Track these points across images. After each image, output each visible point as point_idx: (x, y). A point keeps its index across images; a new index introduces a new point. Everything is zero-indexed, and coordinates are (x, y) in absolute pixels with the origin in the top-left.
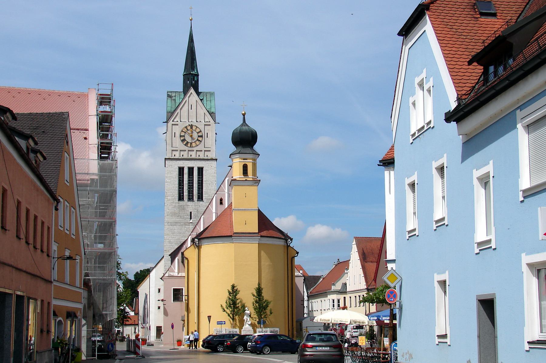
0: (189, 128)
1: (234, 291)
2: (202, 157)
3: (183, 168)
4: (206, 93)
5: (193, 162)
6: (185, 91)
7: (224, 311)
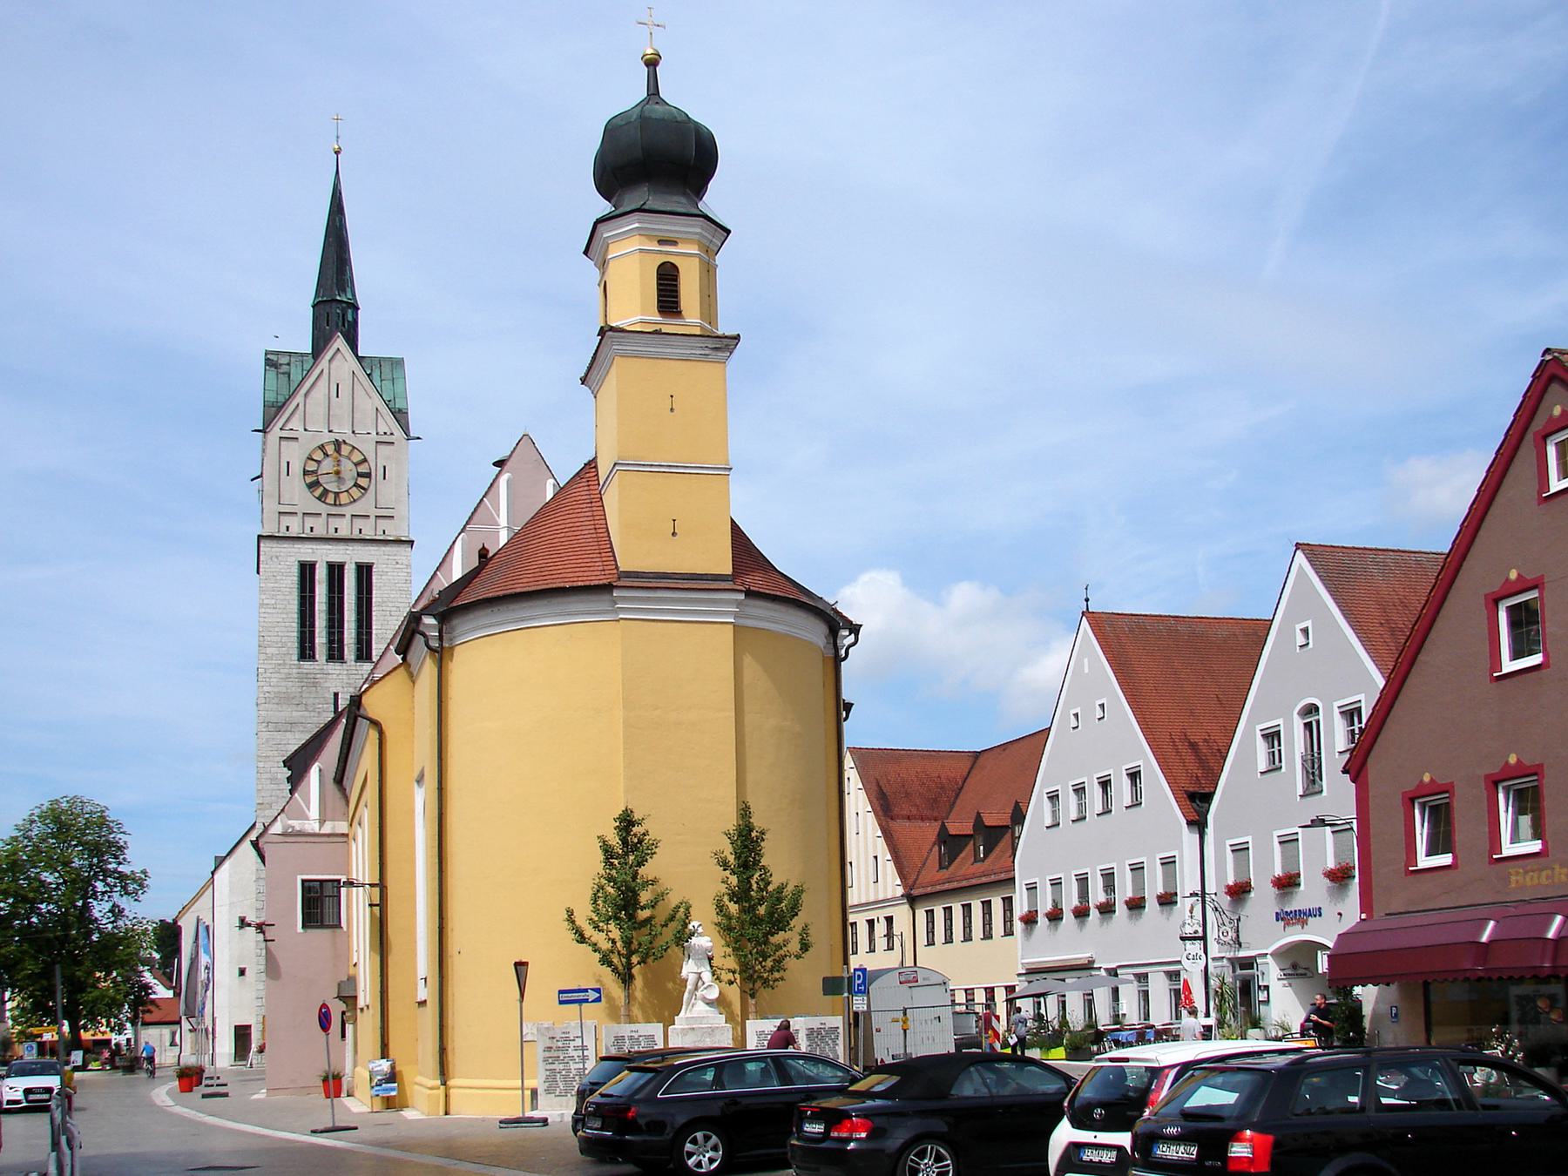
0: (330, 449)
1: (629, 845)
2: (368, 533)
3: (312, 566)
4: (380, 360)
5: (341, 547)
6: (320, 343)
7: (582, 939)
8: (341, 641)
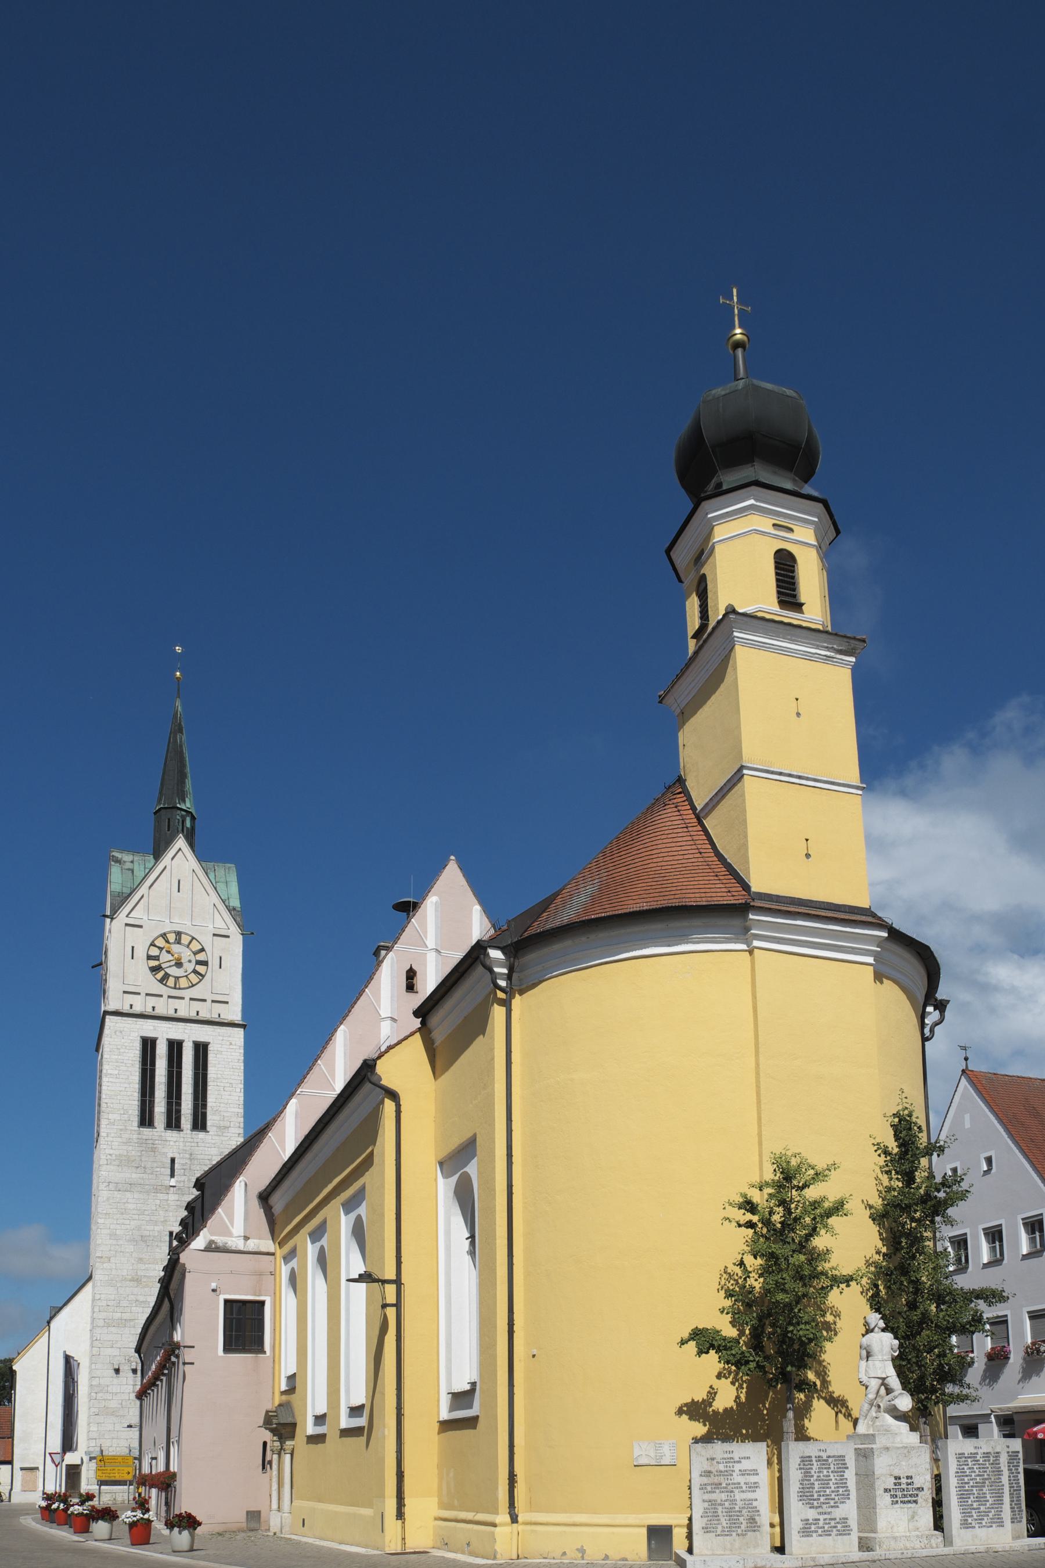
8: (179, 1111)
